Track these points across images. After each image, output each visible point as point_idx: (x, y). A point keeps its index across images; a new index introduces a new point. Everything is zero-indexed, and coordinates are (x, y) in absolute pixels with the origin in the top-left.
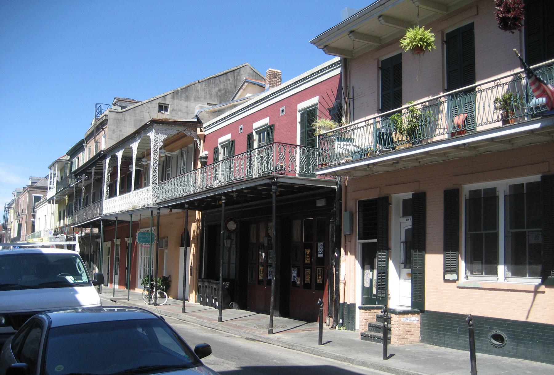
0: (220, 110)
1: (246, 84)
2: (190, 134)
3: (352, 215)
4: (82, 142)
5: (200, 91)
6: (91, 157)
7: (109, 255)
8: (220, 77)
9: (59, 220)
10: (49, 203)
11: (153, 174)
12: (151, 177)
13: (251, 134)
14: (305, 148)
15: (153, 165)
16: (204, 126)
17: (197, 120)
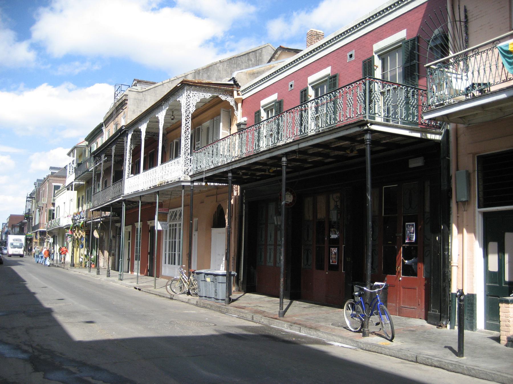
0: (259, 72)
1: (279, 53)
2: (226, 99)
3: (468, 175)
4: (101, 126)
5: (221, 71)
6: (110, 136)
7: (129, 240)
8: (242, 57)
9: (78, 207)
10: (68, 189)
11: (185, 143)
12: (182, 147)
13: (306, 90)
14: (403, 87)
15: (185, 133)
16: (242, 89)
17: (234, 82)
